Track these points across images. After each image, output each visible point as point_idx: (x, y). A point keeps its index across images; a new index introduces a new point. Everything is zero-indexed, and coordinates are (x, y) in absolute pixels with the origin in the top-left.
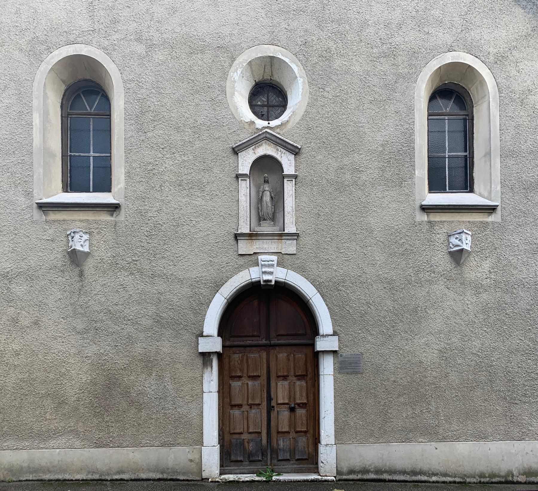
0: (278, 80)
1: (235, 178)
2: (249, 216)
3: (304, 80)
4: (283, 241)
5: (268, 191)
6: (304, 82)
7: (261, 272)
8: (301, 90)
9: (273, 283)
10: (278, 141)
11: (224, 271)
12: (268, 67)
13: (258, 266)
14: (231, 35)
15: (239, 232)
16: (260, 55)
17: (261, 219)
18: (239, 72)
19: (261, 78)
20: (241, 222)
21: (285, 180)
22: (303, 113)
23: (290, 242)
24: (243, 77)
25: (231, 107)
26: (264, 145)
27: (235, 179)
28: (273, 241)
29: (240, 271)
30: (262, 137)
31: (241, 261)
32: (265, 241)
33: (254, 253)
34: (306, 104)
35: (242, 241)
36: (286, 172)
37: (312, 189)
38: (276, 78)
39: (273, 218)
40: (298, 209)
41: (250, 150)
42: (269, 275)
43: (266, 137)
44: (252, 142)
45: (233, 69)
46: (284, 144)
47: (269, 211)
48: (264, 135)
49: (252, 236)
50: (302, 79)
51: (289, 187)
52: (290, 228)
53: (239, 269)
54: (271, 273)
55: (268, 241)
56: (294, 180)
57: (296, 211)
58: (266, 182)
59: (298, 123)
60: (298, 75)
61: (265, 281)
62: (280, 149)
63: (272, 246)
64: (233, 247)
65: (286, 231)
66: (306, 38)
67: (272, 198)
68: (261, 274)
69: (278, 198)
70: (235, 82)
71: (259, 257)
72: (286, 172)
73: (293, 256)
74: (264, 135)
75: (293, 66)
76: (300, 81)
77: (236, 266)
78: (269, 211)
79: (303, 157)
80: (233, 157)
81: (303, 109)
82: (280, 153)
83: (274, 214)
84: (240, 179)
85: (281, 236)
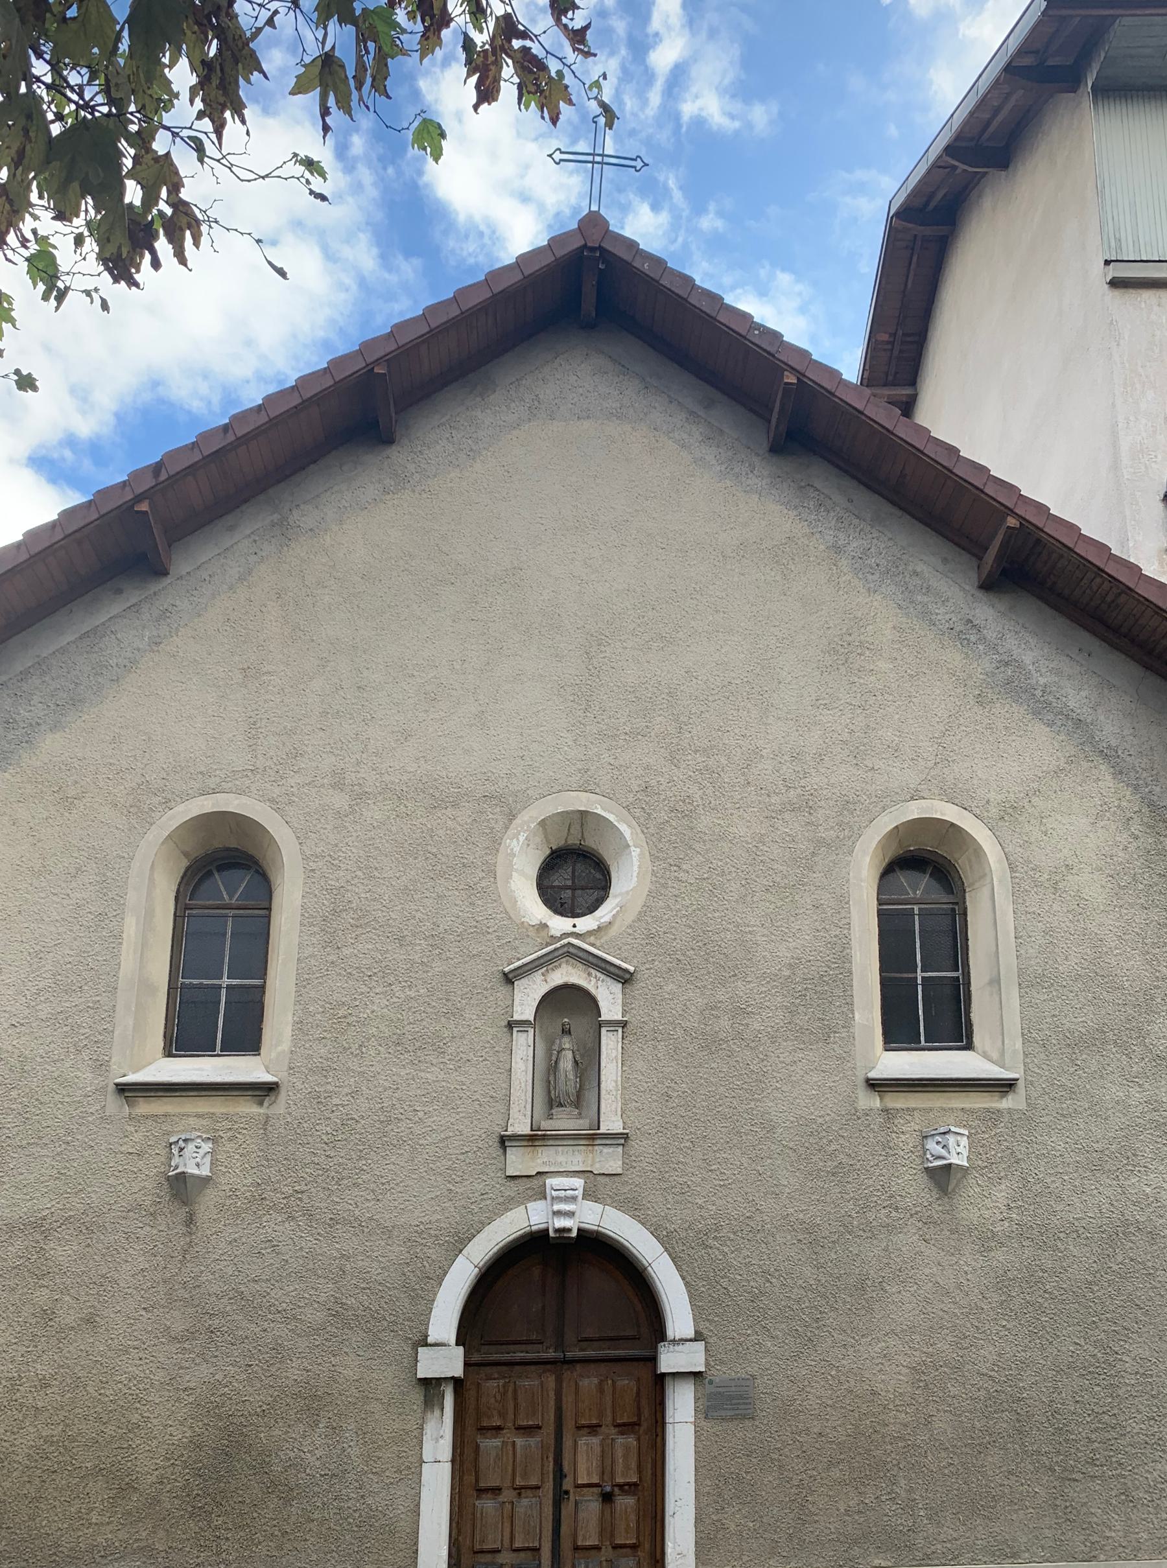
6: (641, 855)
8: (636, 868)
9: (574, 1234)
10: (591, 959)
14: (509, 775)
17: (553, 1103)
21: (603, 1030)
23: (611, 1150)
26: (564, 965)
27: (505, 1030)
29: (507, 1210)
30: (561, 952)
31: (512, 1189)
32: (560, 1148)
33: (538, 1173)
36: (605, 1016)
41: (538, 976)
45: (510, 832)
46: (603, 965)
47: (569, 1089)
49: (535, 1139)
50: (638, 850)
51: (610, 1044)
52: (611, 1123)
53: (506, 1205)
54: (570, 1214)
56: (620, 1030)
57: (624, 1088)
60: (631, 843)
61: (557, 1231)
63: (575, 1158)
69: (588, 1063)
72: (605, 1016)
73: (616, 1178)
74: (565, 949)
75: (623, 827)
76: (635, 852)
80: (504, 990)
81: (640, 902)
85: (593, 1138)
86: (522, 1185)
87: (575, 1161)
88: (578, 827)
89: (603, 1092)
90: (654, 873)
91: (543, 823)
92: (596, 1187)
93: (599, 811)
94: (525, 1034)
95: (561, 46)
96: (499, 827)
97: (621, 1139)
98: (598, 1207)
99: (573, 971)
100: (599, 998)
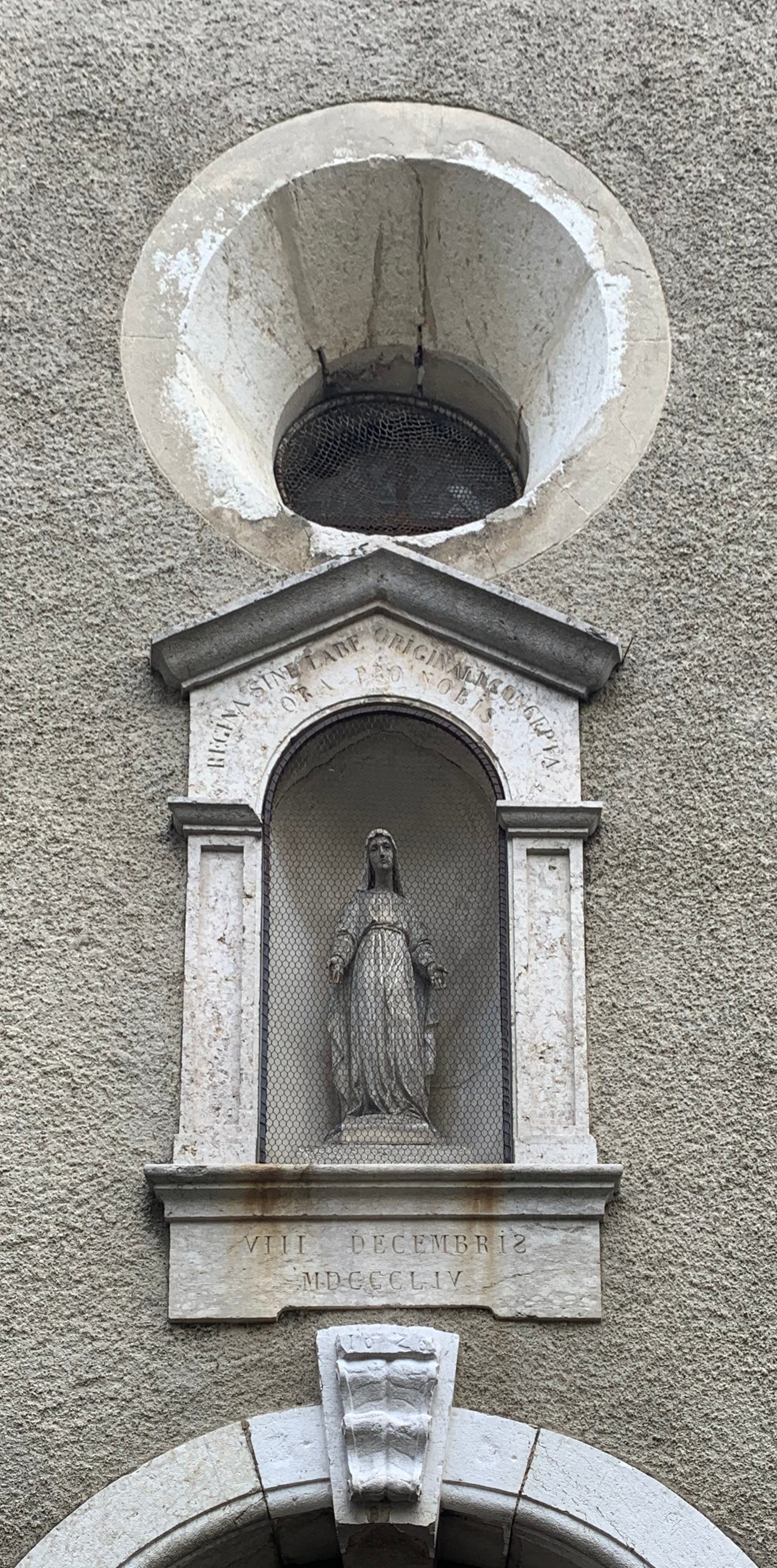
0: (467, 352)
1: (161, 838)
2: (253, 1071)
3: (635, 285)
4: (502, 1229)
5: (392, 927)
6: (636, 297)
7: (336, 1442)
8: (616, 340)
9: (428, 1515)
10: (463, 609)
11: (62, 1434)
12: (401, 256)
13: (317, 1399)
14: (157, 52)
15: (182, 1162)
16: (343, 157)
17: (340, 1105)
18: (208, 246)
19: (358, 338)
20: (196, 1109)
21: (517, 851)
22: (633, 465)
23: (556, 1237)
24: (235, 293)
25: (146, 436)
26: (367, 643)
27: (163, 848)
28: (428, 1229)
29: (175, 1437)
30: (352, 588)
31: (189, 1369)
32: (368, 1231)
33: (291, 1314)
34: (658, 415)
35: (198, 1230)
36: (519, 791)
37: (706, 908)
38: (454, 337)
39: (433, 1104)
40: (608, 1031)
41: (274, 678)
42: (398, 1459)
43: (381, 595)
44: (287, 615)
45: (165, 230)
46: (509, 629)
47: (400, 1079)
48: (370, 580)
49: (264, 1196)
50: (623, 283)
51: (543, 899)
52: (554, 1136)
53: (172, 1422)
54: (414, 1443)
55: (389, 1231)
56: (577, 851)
57: (596, 1040)
58: (383, 878)
59: (602, 521)
60: (595, 260)
61: (363, 1499)
62: (476, 666)
63: (429, 1264)
64: (129, 1274)
65: (523, 1162)
66: (647, 59)
67: (421, 978)
68: (334, 1454)
69: (467, 983)
70: (178, 299)
71: (321, 1334)
72: (519, 791)
73: (579, 1337)
74: (370, 580)
75: (567, 213)
76: (612, 292)
77: (152, 1403)
78: (400, 1079)
79: (636, 721)
80: (147, 728)
81: (637, 445)
82: (475, 692)
83: (436, 1083)
84: (195, 844)
85: (495, 1193)
86: (230, 1353)
87: (425, 1271)
88: (410, 264)
89: (521, 1053)
90: (680, 349)
91: (281, 206)
92: (506, 1359)
93: (479, 161)
94: (230, 863)
95: (422, 541)
96: (122, 209)
97: (590, 1198)
98: (516, 1434)
99: (401, 660)
100: (496, 745)
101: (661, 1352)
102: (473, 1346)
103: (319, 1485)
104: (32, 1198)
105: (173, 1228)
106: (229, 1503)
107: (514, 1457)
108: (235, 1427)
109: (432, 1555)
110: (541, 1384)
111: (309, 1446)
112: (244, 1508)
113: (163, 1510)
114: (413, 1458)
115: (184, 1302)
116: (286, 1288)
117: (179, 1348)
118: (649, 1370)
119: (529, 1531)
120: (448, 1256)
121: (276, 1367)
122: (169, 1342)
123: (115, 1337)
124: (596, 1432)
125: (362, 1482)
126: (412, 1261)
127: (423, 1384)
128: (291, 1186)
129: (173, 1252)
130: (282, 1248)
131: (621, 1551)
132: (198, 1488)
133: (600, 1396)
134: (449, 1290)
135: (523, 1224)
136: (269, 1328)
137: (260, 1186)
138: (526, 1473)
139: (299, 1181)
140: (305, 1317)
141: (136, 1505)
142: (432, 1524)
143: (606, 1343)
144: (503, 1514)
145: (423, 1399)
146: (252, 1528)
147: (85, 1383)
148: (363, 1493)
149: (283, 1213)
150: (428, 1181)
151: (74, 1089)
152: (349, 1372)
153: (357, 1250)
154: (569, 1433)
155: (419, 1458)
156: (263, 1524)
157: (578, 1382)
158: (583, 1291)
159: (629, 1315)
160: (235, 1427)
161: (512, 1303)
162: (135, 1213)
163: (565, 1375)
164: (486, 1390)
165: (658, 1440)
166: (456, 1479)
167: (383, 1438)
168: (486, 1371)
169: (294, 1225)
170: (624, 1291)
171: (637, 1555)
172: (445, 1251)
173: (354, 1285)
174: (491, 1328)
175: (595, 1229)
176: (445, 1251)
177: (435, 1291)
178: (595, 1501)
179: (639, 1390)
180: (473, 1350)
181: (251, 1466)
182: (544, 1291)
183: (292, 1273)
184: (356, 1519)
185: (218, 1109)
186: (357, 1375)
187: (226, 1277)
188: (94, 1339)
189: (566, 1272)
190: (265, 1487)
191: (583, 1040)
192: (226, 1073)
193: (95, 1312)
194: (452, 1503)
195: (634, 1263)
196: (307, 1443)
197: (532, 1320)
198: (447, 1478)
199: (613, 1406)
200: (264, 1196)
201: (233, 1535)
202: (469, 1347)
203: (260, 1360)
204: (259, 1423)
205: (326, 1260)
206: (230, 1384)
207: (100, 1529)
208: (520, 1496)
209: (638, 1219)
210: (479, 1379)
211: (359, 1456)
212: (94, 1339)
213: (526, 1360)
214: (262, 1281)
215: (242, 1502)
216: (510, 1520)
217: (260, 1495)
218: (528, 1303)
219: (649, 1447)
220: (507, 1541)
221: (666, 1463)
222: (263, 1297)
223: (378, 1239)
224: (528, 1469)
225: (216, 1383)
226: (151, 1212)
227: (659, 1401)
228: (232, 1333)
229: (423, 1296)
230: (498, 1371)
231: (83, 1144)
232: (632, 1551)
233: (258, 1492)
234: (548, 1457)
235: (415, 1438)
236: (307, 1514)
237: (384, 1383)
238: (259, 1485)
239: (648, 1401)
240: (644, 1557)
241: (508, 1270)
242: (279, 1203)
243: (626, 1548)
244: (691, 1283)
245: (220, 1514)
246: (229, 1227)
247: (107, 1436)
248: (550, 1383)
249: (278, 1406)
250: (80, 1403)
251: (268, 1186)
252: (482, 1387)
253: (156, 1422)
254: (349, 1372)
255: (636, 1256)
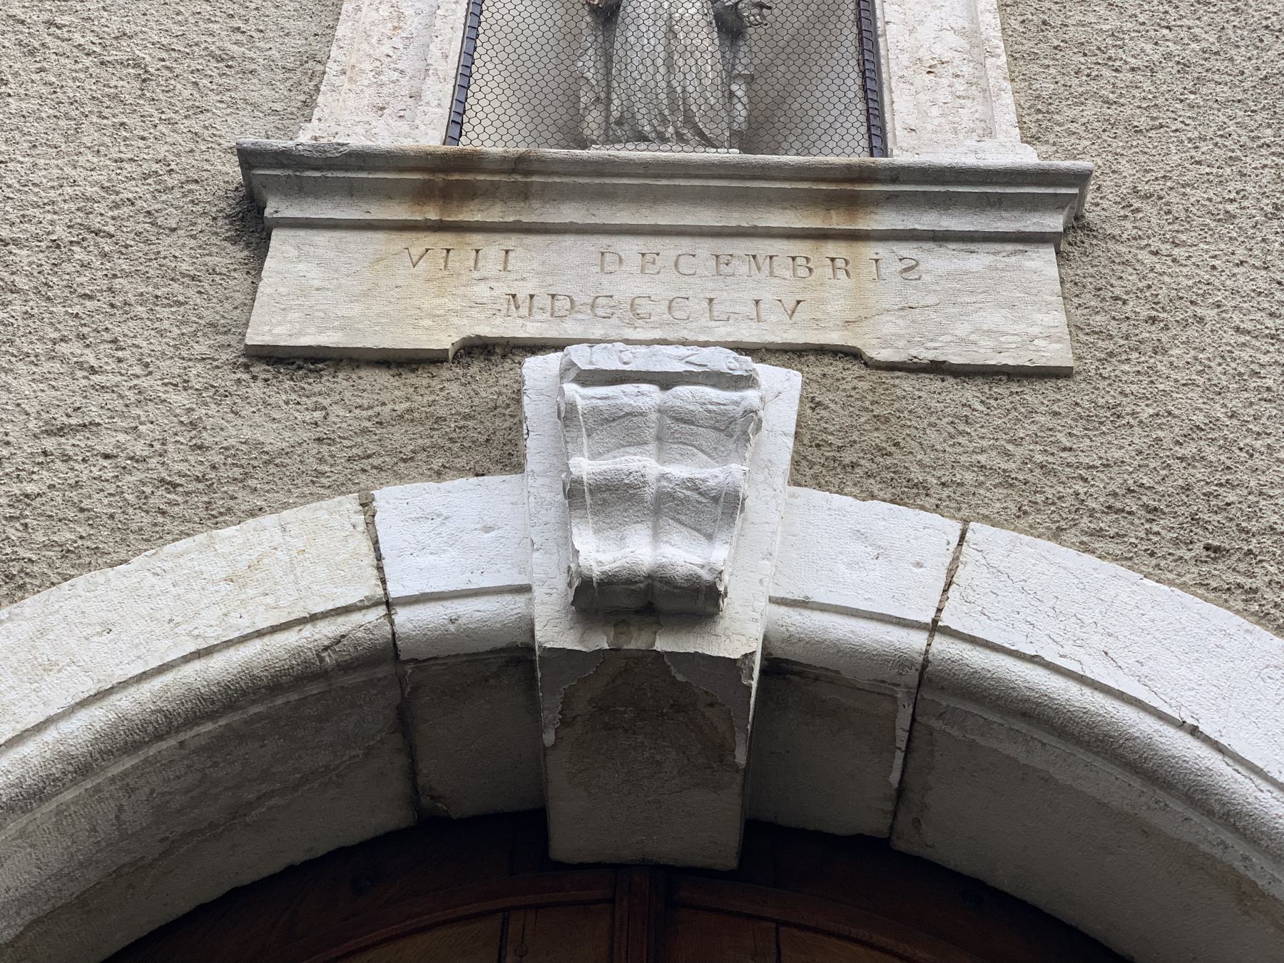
4: (872, 250)
23: (979, 260)
31: (272, 417)
32: (630, 247)
33: (479, 350)
49: (445, 189)
53: (214, 493)
55: (669, 248)
61: (596, 598)
73: (1034, 395)
77: (179, 462)
85: (862, 196)
101: (1199, 419)
102: (827, 402)
103: (508, 598)
104: (36, 194)
105: (277, 237)
106: (313, 618)
107: (919, 565)
108: (350, 503)
109: (741, 757)
110: (963, 459)
111: (492, 534)
112: (343, 630)
113: (167, 627)
114: (710, 537)
115: (280, 324)
116: (473, 312)
117: (257, 390)
118: (1178, 443)
119: (953, 703)
120: (777, 281)
121: (439, 419)
122: (239, 381)
123: (138, 370)
124: (1084, 533)
125: (600, 563)
126: (710, 285)
127: (733, 420)
128: (496, 178)
129: (269, 263)
130: (472, 263)
131: (1170, 731)
132: (251, 592)
133: (1086, 480)
134: (780, 322)
135: (915, 245)
136: (434, 370)
137: (440, 177)
138: (945, 591)
139: (513, 171)
140: (504, 356)
141: (113, 617)
142: (748, 656)
143: (1086, 404)
144: (901, 662)
145: (732, 446)
146: (356, 678)
147: (61, 431)
148: (601, 583)
149: (478, 217)
150: (743, 178)
151: (144, 81)
152: (583, 397)
153: (607, 269)
154: (1031, 530)
155: (722, 536)
156: (383, 671)
157: (1039, 458)
158: (1035, 330)
159: (1126, 367)
160: (350, 503)
161: (901, 343)
162: (214, 219)
163: (1010, 447)
164: (853, 465)
165: (1217, 549)
166: (797, 595)
167: (648, 498)
168: (855, 437)
169: (497, 237)
170: (1111, 337)
171: (1206, 740)
172: (771, 274)
173: (600, 312)
174: (860, 378)
175: (1049, 253)
176: (771, 274)
177: (754, 324)
178: (1097, 641)
179: (1163, 472)
180: (826, 408)
181: (371, 559)
182: (962, 330)
183: (488, 293)
184: (582, 641)
185: (382, 109)
186: (600, 403)
187: (365, 295)
188: (93, 371)
189: (1000, 306)
190: (395, 591)
191: (1001, 51)
192: (402, 72)
193: (107, 336)
194: (789, 640)
195: (1124, 303)
196: (488, 529)
197: (938, 369)
198: (781, 594)
199: (1115, 495)
200: (445, 189)
201: (313, 689)
202: (819, 404)
203: (410, 411)
204: (389, 497)
205: (549, 280)
206: (346, 443)
207: (22, 655)
208: (934, 628)
209: (1123, 249)
210: (840, 449)
211: (597, 531)
212: (93, 371)
213: (930, 425)
214: (428, 303)
215: (341, 620)
216: (912, 677)
217: (382, 610)
218: (929, 344)
219: (1197, 561)
220: (902, 736)
221: (1239, 586)
222: (427, 322)
223: (648, 257)
224: (949, 584)
225: (319, 440)
226: (242, 219)
227: (1207, 489)
228: (362, 373)
229: (729, 329)
230: (878, 438)
231: (143, 138)
232: (1194, 731)
233: (376, 604)
234: (988, 566)
235: (715, 500)
236: (474, 659)
237: (654, 416)
238: (380, 591)
239: (1187, 488)
240: (1223, 741)
241: (891, 300)
242: (473, 205)
243: (1181, 725)
244: (1237, 329)
245: (291, 639)
246: (380, 236)
247: (82, 510)
248: (983, 458)
249: (439, 475)
250: (41, 459)
251: (456, 177)
252: (847, 461)
253: (187, 493)
254: (583, 397)
255: (1127, 293)
